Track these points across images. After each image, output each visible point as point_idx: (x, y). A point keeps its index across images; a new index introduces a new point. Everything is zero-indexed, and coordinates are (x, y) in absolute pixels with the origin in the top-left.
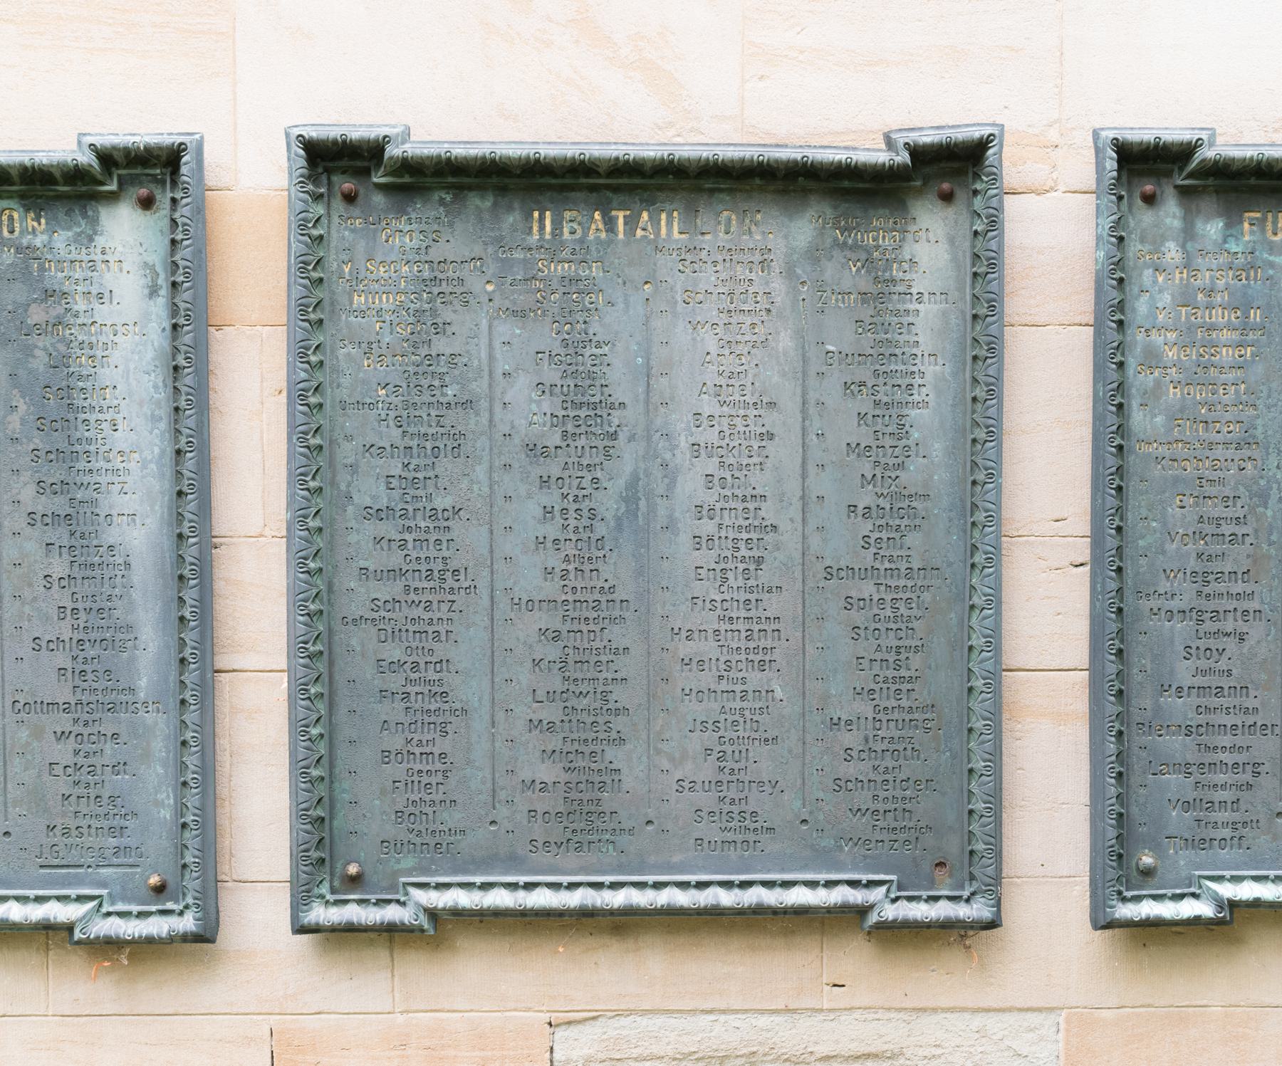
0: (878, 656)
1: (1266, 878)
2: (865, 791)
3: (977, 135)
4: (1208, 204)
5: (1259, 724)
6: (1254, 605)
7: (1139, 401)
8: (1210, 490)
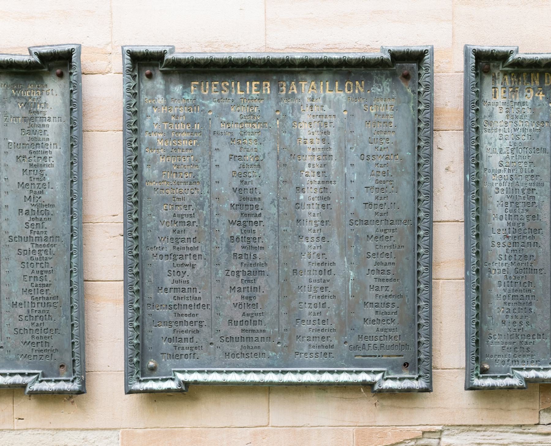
0: (33, 275)
1: (203, 371)
2: (28, 334)
3: (66, 49)
4: (175, 78)
5: (201, 304)
6: (198, 252)
7: (147, 164)
8: (179, 203)
